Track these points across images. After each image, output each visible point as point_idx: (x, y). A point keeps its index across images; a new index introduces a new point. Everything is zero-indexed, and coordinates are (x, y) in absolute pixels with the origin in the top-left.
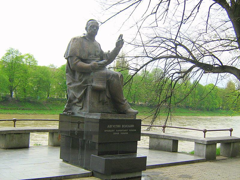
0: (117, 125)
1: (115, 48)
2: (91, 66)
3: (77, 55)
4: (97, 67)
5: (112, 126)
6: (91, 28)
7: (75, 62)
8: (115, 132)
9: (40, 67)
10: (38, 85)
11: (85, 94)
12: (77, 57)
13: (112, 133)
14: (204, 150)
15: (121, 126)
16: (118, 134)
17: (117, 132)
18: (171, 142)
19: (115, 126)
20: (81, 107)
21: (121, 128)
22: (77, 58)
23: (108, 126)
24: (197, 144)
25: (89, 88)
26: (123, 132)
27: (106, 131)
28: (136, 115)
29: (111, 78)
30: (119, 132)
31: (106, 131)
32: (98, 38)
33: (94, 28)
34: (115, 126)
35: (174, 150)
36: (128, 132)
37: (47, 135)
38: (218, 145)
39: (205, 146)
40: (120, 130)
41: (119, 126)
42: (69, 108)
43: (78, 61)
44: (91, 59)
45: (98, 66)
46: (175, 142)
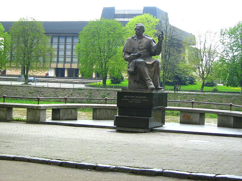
13: (128, 101)
17: (132, 101)
18: (198, 115)
21: (135, 98)
26: (136, 101)
27: (122, 99)
30: (133, 101)
36: (141, 101)
40: (134, 100)
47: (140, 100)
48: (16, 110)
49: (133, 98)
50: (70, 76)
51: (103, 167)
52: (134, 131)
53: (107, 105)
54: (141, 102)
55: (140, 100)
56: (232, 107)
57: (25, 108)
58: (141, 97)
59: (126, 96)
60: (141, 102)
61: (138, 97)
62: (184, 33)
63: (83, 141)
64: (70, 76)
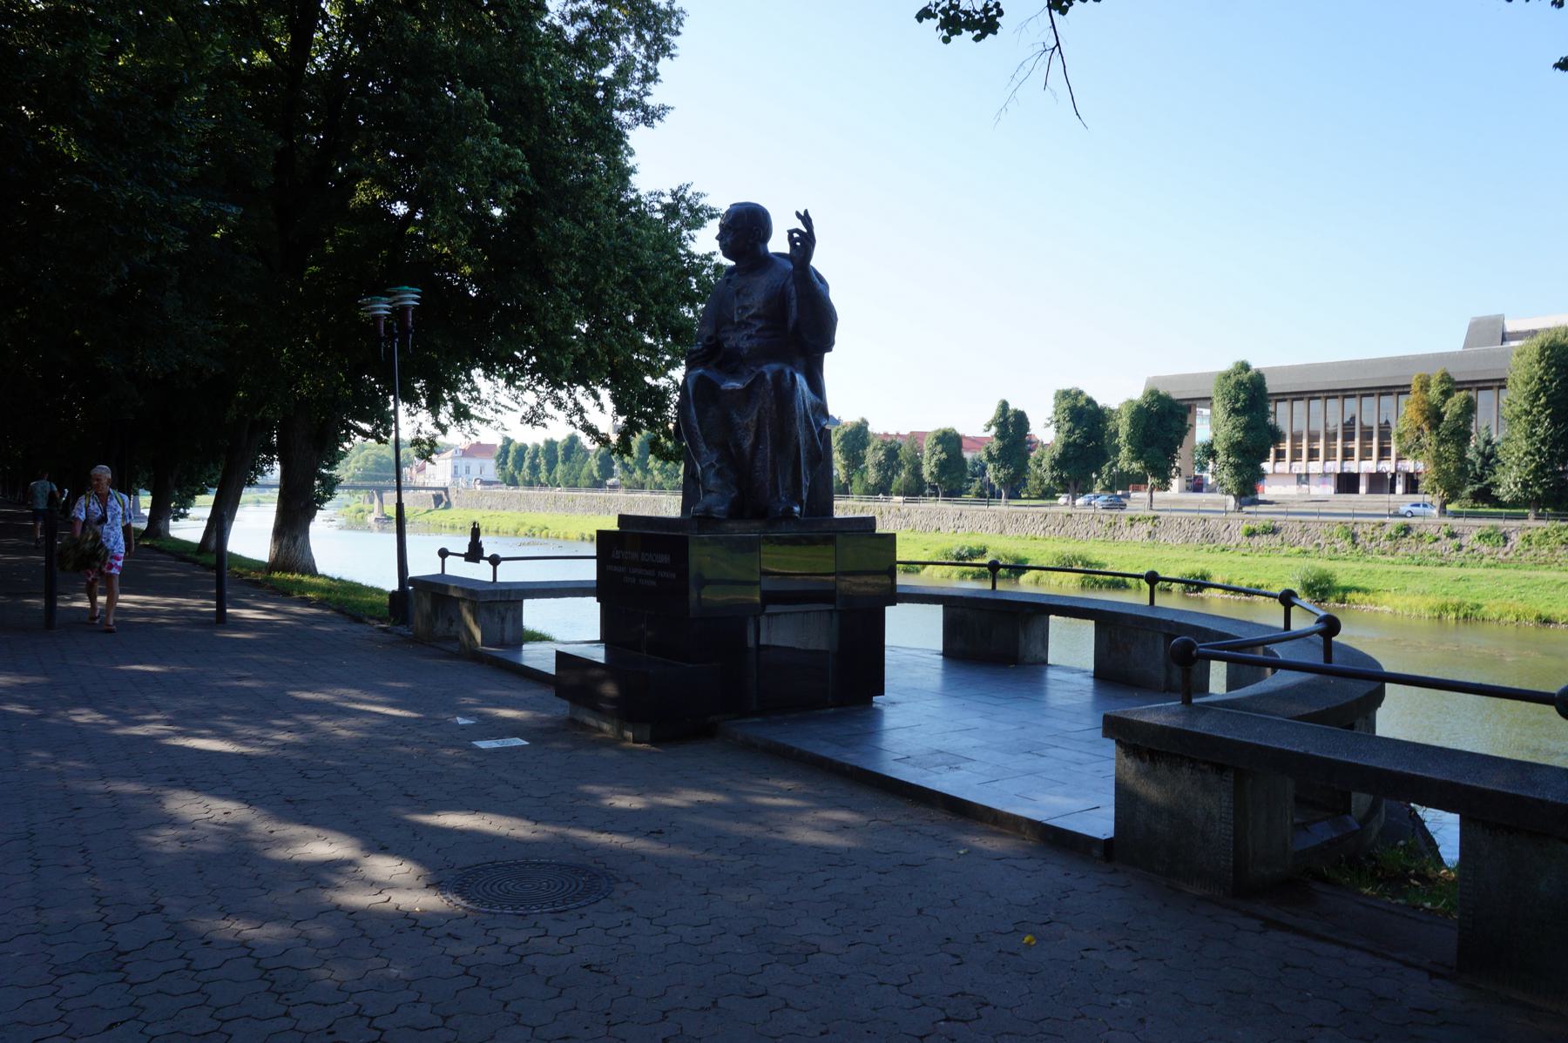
50: (1371, 491)
64: (1371, 491)
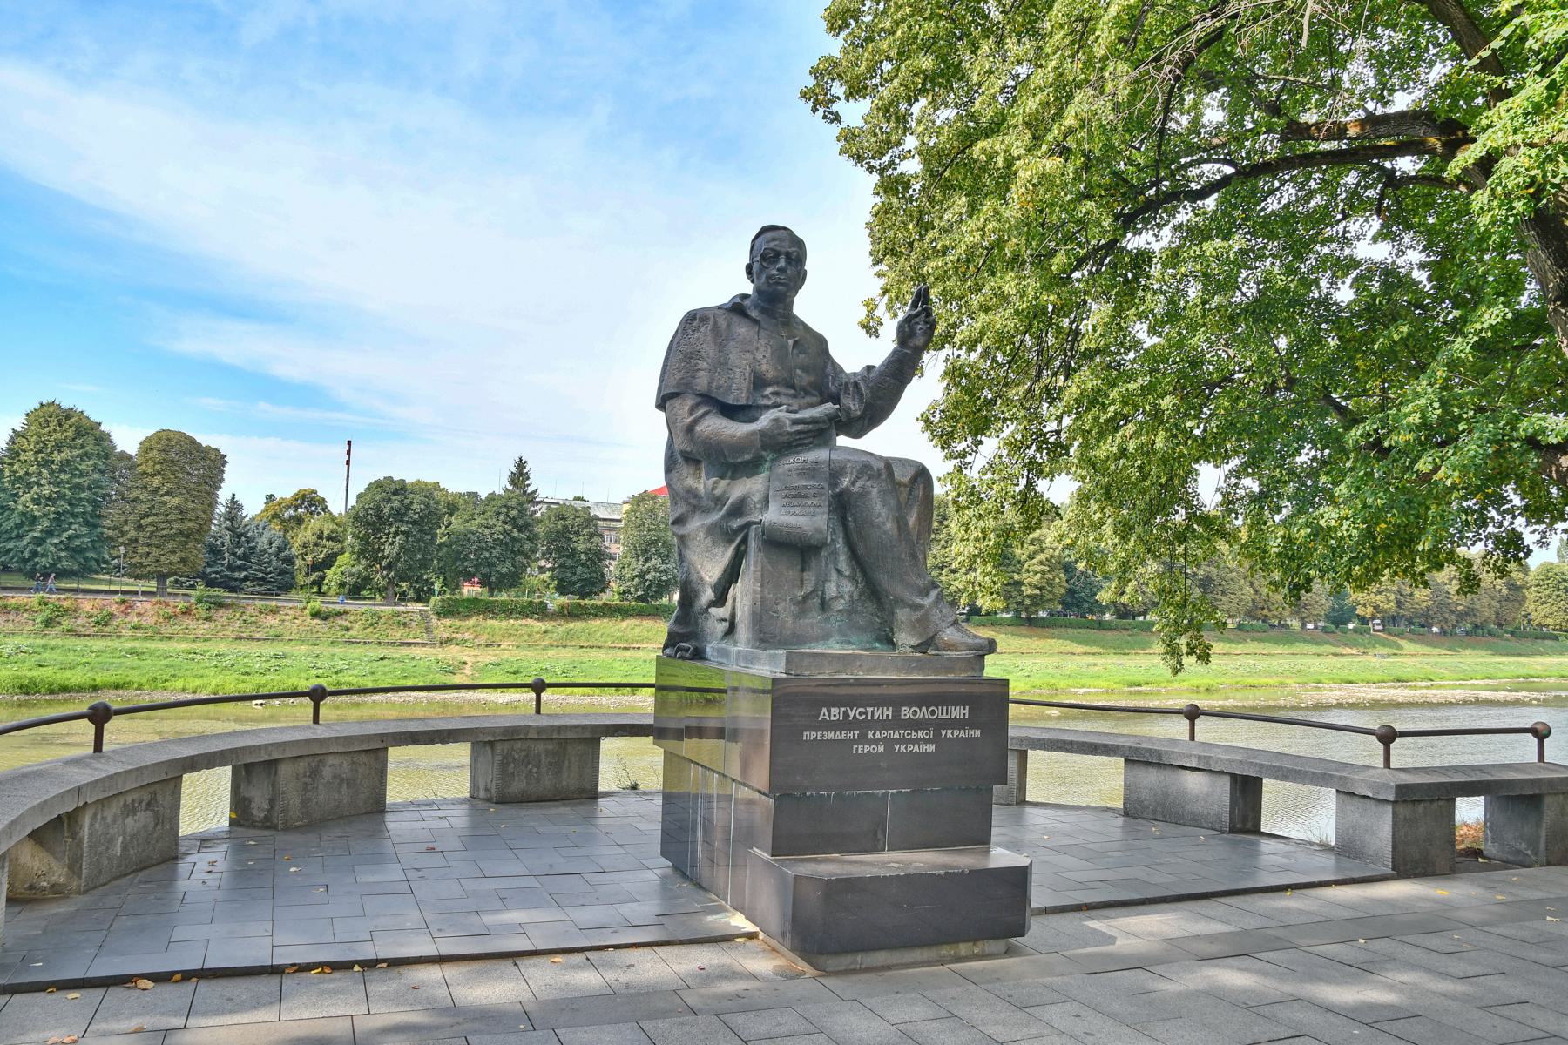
0: (870, 709)
1: (895, 351)
2: (763, 433)
3: (698, 388)
4: (788, 433)
5: (846, 713)
6: (765, 264)
7: (689, 420)
8: (863, 739)
9: (882, 365)
10: (1323, 379)
11: (738, 557)
12: (700, 395)
13: (854, 742)
14: (1381, 830)
15: (897, 713)
16: (881, 749)
17: (876, 742)
19: (861, 714)
20: (727, 624)
21: (897, 723)
22: (699, 399)
23: (824, 710)
24: (1344, 797)
25: (752, 534)
26: (904, 741)
27: (808, 736)
28: (982, 656)
29: (853, 483)
30: (886, 741)
31: (808, 736)
32: (806, 306)
33: (777, 262)
34: (861, 714)
35: (1249, 825)
36: (936, 739)
37: (461, 753)
38: (1470, 812)
39: (1390, 808)
41: (882, 713)
42: (681, 631)
43: (700, 412)
44: (766, 402)
45: (789, 429)
46: (1247, 789)
47: (931, 734)
48: (1112, 799)
49: (884, 725)
51: (723, 581)
52: (283, 371)
53: (1089, 950)
54: (933, 748)
55: (931, 734)
56: (109, 727)
57: (452, 748)
58: (938, 711)
59: (836, 713)
60: (933, 748)
61: (919, 716)
62: (1061, 138)
63: (826, 694)
